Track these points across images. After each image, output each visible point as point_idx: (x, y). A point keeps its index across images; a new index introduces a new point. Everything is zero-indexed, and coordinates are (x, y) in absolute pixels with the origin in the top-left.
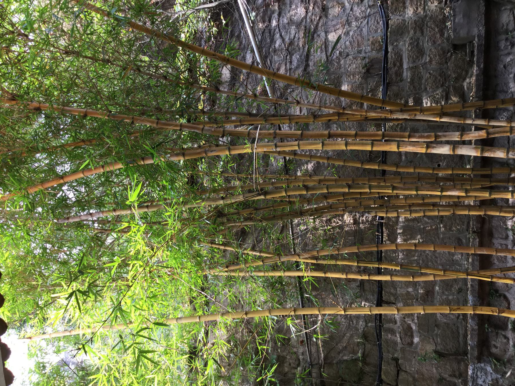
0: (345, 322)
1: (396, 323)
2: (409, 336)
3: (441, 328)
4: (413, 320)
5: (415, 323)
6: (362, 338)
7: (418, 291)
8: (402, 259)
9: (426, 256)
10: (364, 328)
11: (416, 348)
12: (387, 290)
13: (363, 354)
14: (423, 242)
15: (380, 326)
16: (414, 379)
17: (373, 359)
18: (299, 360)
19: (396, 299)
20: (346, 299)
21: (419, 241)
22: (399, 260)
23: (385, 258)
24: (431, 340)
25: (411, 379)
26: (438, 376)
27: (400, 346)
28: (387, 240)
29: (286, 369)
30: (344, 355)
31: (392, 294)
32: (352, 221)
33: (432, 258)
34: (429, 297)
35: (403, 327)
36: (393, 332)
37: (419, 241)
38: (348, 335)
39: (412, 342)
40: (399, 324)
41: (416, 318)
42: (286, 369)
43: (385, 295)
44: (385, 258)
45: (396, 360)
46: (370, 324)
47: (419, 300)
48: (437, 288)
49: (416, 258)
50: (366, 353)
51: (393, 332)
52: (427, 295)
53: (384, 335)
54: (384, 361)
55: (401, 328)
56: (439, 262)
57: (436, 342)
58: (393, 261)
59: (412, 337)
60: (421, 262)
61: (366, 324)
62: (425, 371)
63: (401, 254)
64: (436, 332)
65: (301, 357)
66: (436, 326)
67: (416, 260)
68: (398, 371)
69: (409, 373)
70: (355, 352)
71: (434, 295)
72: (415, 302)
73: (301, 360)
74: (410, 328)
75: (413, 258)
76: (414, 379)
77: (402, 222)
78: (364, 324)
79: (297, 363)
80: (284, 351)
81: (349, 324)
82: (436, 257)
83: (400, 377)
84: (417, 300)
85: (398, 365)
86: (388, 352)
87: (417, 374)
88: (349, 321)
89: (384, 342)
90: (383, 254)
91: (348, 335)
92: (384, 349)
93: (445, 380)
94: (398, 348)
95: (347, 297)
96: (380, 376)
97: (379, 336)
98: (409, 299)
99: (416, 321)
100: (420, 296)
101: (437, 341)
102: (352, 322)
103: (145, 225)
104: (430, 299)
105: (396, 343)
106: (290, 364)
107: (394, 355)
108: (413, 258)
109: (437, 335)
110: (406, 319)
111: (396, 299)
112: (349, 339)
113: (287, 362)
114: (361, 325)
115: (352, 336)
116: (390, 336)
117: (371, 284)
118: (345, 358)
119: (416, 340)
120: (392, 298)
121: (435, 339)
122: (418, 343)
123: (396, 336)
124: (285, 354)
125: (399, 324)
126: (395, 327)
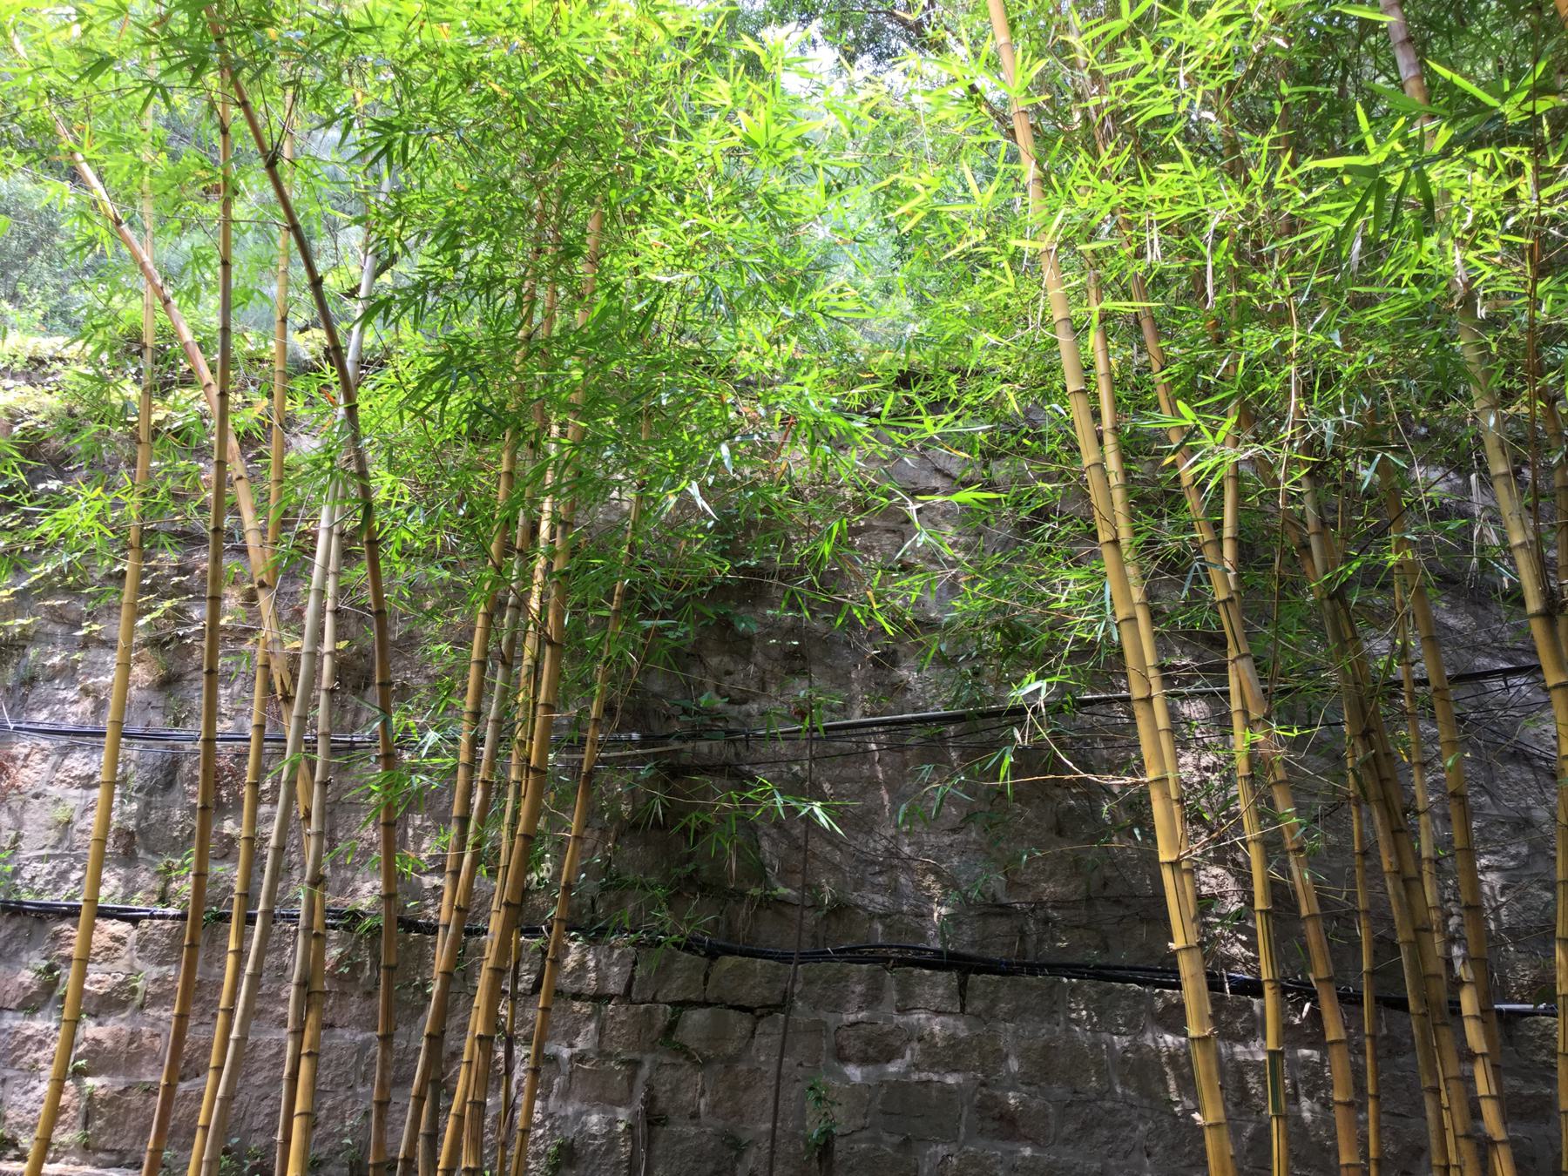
0: (875, 850)
1: (903, 1011)
2: (865, 1052)
3: (900, 1156)
4: (917, 1067)
5: (907, 1074)
6: (834, 900)
7: (1013, 1088)
8: (1111, 1046)
9: (1128, 1124)
10: (864, 908)
11: (830, 1071)
12: (1004, 990)
13: (783, 902)
14: (1175, 1115)
15: (887, 959)
16: (730, 1061)
17: (771, 933)
18: (745, 702)
19: (978, 1016)
20: (949, 857)
21: (1176, 1104)
22: (1105, 1036)
23: (1109, 992)
24: (860, 1122)
25: (730, 1049)
26: (746, 1137)
27: (831, 1019)
28: (1166, 1001)
29: (714, 661)
30: (774, 843)
31: (994, 1003)
32: (1204, 889)
33: (1124, 1141)
34: (996, 1125)
35: (891, 1033)
36: (872, 998)
37: (1176, 1104)
38: (838, 857)
39: (845, 1060)
40: (900, 1019)
41: (924, 1076)
42: (714, 661)
43: (988, 984)
44: (1109, 992)
45: (783, 1004)
46: (880, 928)
47: (984, 1090)
48: (1027, 1152)
49: (1119, 1090)
50: (787, 911)
51: (872, 998)
52: (1002, 1117)
53: (860, 971)
54: (777, 968)
55: (887, 1028)
56: (1112, 1162)
57: (856, 1136)
58: (1099, 1015)
59: (863, 1061)
60: (1108, 1105)
61: (880, 916)
62: (760, 1097)
63: (1125, 1041)
64: (886, 1136)
65: (753, 707)
66: (907, 1141)
67: (1112, 1090)
68: (750, 1010)
69: (748, 1046)
70: (786, 874)
71: (1003, 1139)
72: (975, 1078)
73: (744, 707)
74: (891, 1055)
75: (1116, 1081)
76: (730, 1061)
77: (1233, 1054)
78: (879, 910)
79: (735, 694)
80: (767, 656)
81: (873, 863)
82: (1126, 1155)
83: (733, 1015)
84: (983, 1084)
85: (770, 1009)
86: (809, 982)
87: (750, 1071)
88: (881, 864)
89: (839, 971)
90: (1119, 985)
91: (838, 857)
92: (816, 968)
93: (738, 1158)
94: (823, 1015)
95: (955, 861)
96: (730, 952)
97: (855, 955)
98: (983, 1057)
99: (915, 1077)
100: (998, 1093)
101: (859, 1141)
102: (880, 873)
103: (743, 321)
104: (991, 1125)
105: (838, 1006)
106: (728, 673)
107: (801, 999)
108: (1116, 1081)
109: (876, 1140)
110: (916, 1046)
111: (978, 1016)
112: (826, 861)
113: (736, 663)
114: (871, 901)
115: (836, 868)
116: (859, 989)
117: (1007, 940)
118: (765, 844)
119: (855, 1073)
120: (978, 1005)
121: (865, 1134)
122: (847, 1080)
123: (860, 1009)
124: (759, 658)
125: (900, 1019)
126: (887, 1008)
